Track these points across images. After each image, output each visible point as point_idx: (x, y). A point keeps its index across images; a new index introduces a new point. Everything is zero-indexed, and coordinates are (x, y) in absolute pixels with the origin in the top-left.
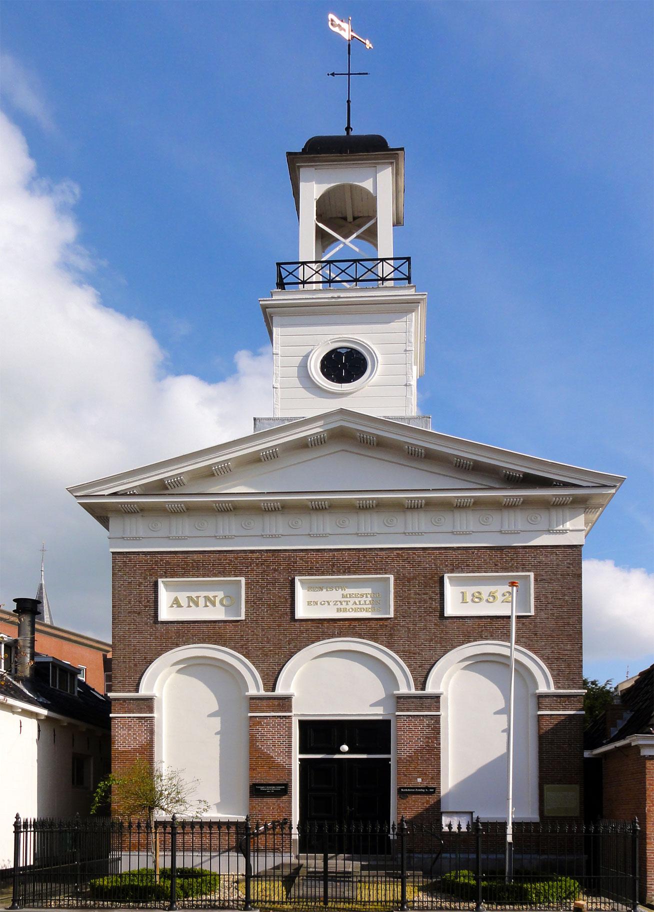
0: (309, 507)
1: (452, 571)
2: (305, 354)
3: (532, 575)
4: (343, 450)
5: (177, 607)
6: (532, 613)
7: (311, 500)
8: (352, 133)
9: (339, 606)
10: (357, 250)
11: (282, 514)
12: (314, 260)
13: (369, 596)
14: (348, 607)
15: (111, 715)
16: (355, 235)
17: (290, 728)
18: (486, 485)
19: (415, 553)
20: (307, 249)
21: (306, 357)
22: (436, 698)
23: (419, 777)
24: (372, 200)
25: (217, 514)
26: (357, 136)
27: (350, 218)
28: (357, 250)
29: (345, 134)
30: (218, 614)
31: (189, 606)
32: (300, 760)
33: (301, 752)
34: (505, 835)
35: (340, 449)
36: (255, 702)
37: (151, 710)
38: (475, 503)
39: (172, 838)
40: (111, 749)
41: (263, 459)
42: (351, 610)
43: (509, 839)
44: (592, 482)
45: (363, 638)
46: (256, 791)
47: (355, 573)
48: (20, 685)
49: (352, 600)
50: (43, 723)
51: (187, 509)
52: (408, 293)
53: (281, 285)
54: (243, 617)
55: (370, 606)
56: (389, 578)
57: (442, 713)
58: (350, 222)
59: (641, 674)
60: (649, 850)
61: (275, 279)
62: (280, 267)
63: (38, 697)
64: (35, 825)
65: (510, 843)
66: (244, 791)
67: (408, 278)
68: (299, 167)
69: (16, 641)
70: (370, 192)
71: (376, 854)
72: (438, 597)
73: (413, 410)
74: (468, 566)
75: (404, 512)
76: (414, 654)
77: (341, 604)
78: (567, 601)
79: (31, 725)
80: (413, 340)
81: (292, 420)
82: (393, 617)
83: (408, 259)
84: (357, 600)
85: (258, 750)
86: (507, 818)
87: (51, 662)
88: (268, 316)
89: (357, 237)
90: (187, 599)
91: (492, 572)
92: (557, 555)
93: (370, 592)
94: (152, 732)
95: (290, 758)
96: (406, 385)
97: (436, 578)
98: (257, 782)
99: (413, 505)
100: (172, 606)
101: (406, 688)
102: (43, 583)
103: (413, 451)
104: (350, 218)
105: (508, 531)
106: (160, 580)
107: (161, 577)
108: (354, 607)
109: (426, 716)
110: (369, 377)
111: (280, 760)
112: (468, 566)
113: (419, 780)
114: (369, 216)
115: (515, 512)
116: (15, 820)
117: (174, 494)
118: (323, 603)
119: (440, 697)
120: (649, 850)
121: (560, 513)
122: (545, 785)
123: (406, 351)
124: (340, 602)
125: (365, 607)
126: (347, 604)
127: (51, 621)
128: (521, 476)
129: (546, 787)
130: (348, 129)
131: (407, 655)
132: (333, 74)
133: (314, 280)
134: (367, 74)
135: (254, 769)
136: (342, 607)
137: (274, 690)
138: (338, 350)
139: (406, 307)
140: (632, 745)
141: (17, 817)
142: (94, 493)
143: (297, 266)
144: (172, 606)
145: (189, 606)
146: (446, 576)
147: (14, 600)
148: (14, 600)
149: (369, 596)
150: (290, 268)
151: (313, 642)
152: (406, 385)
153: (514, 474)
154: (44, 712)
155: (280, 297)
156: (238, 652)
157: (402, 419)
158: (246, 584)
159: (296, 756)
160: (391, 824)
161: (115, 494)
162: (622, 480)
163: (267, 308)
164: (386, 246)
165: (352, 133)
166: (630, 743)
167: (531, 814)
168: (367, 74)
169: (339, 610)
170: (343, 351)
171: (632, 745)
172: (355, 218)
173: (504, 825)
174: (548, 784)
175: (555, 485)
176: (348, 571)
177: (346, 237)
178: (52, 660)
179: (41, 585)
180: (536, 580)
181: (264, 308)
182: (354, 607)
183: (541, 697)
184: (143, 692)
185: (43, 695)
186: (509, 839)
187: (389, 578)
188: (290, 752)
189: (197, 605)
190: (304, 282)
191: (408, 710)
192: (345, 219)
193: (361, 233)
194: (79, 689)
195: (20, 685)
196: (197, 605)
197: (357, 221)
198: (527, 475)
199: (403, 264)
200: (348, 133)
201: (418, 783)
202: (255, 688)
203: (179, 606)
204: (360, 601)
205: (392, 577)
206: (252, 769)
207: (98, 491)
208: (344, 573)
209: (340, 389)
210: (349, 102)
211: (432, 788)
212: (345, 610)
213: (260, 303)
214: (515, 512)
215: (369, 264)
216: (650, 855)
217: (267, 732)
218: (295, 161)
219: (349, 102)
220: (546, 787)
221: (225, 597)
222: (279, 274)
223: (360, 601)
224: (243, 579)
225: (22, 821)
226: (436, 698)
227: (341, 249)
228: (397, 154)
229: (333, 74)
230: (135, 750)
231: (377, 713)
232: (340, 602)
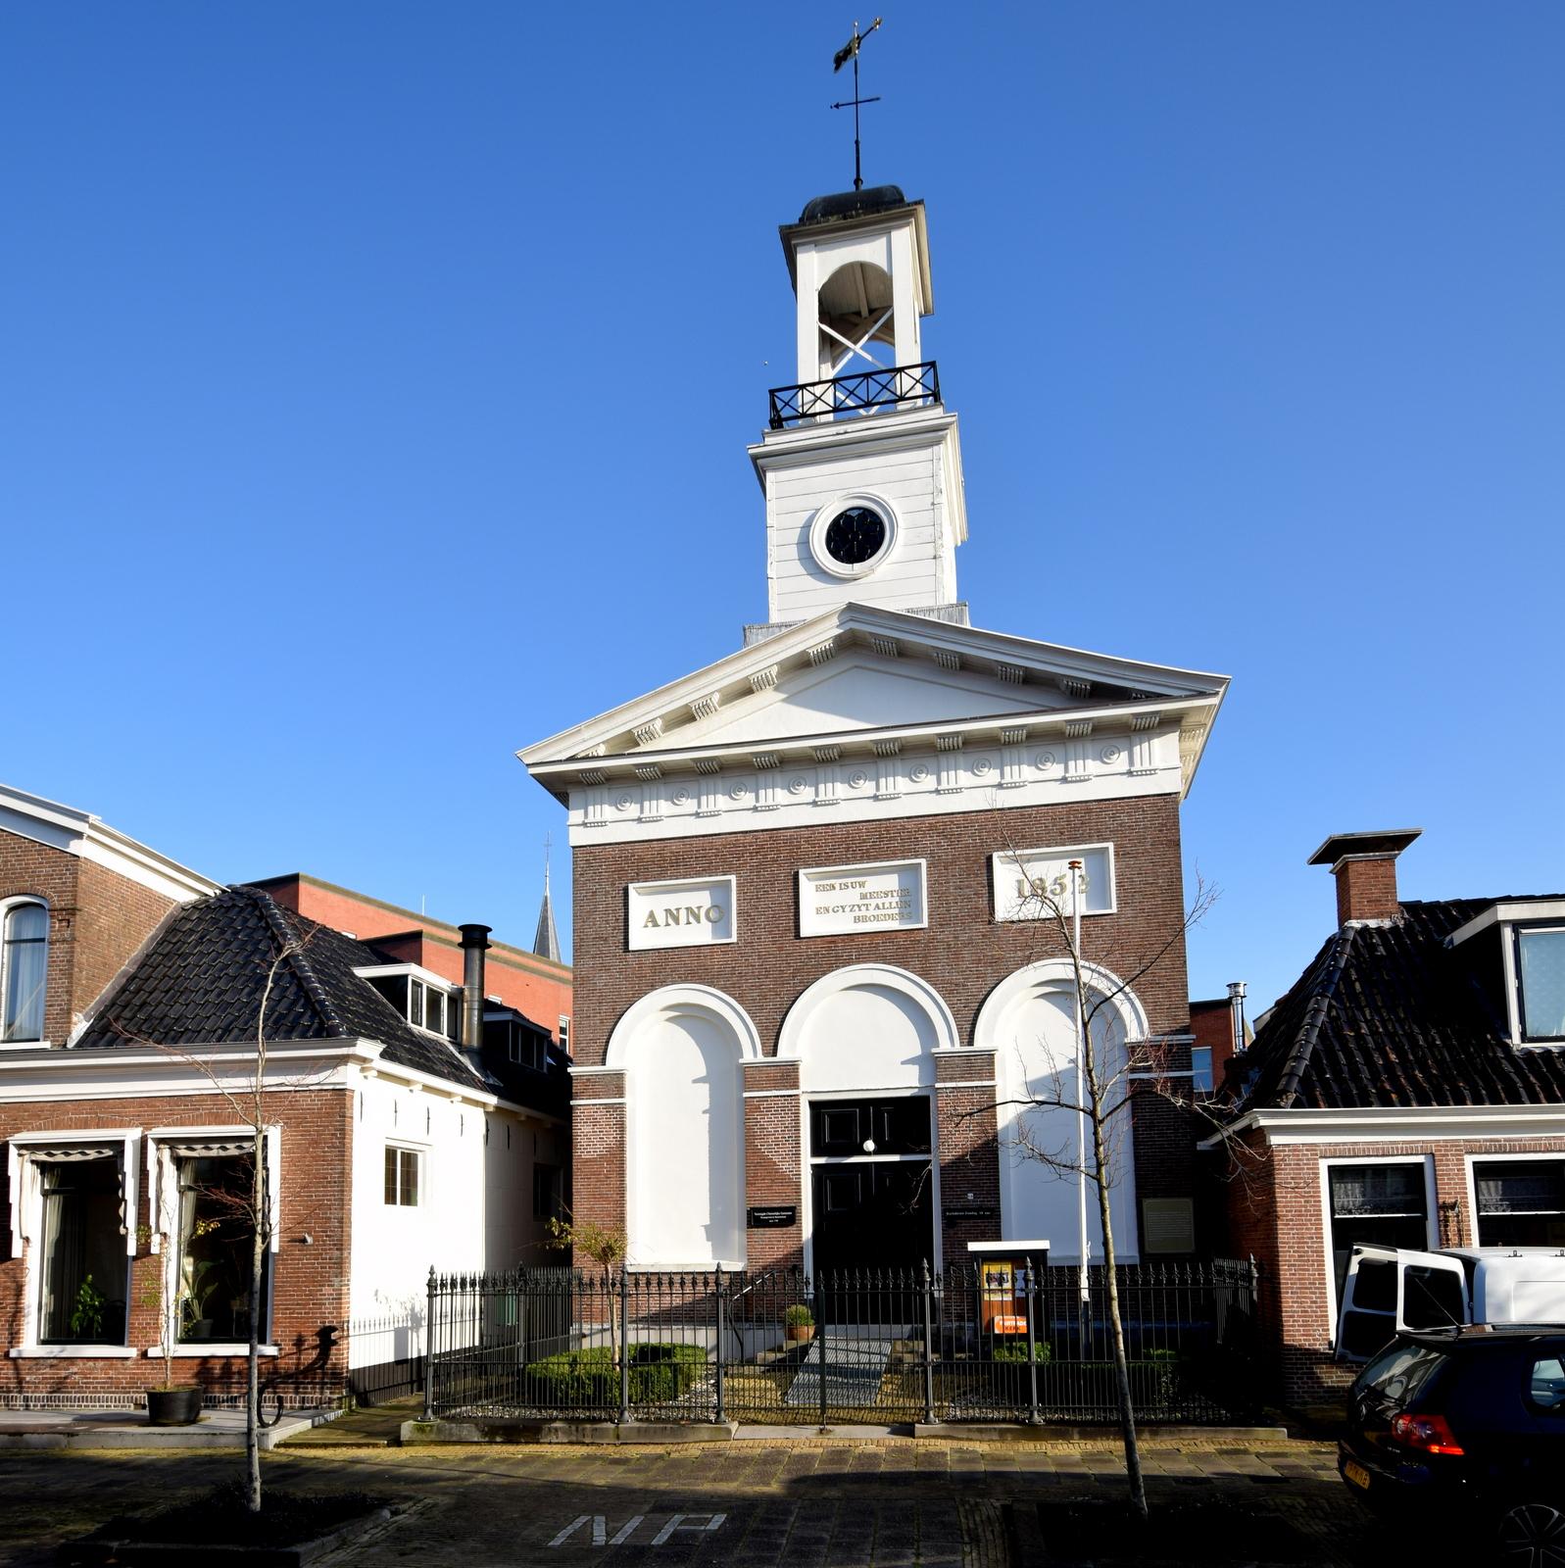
0: (814, 760)
1: (809, 866)
2: (803, 522)
3: (1111, 846)
4: (856, 667)
5: (653, 926)
6: (1114, 910)
7: (816, 748)
8: (863, 187)
9: (857, 913)
10: (869, 358)
11: (841, 766)
12: (920, 362)
13: (895, 894)
14: (868, 914)
15: (572, 1103)
16: (866, 337)
17: (797, 1115)
18: (1043, 706)
19: (952, 822)
20: (810, 365)
21: (807, 527)
22: (988, 1058)
23: (970, 1191)
24: (885, 280)
25: (586, 788)
26: (841, 195)
27: (865, 312)
28: (869, 358)
29: (853, 188)
30: (701, 934)
31: (668, 925)
32: (815, 1167)
33: (815, 1153)
34: (1078, 1290)
35: (846, 668)
36: (750, 1076)
37: (620, 1093)
38: (1030, 736)
39: (623, 1301)
40: (572, 1156)
41: (754, 688)
42: (872, 918)
43: (1085, 1295)
44: (1030, 703)
45: (889, 964)
46: (756, 1219)
47: (876, 859)
48: (465, 1060)
49: (873, 902)
50: (493, 1116)
51: (721, 768)
52: (935, 415)
53: (777, 423)
54: (734, 939)
55: (897, 911)
56: (1107, 848)
57: (627, 1100)
58: (866, 318)
59: (1278, 1003)
60: (1286, 1311)
61: (766, 414)
62: (774, 395)
63: (487, 1076)
64: (484, 1283)
65: (1086, 1303)
66: (738, 1216)
67: (936, 396)
68: (796, 246)
69: (461, 991)
70: (883, 271)
71: (900, 1323)
72: (985, 890)
73: (950, 595)
74: (1023, 837)
75: (1000, 750)
76: (956, 985)
77: (860, 910)
78: (1161, 886)
79: (477, 1121)
80: (943, 487)
81: (791, 626)
82: (927, 926)
83: (772, 392)
84: (880, 902)
85: (756, 1151)
86: (1079, 1258)
87: (511, 1021)
88: (760, 467)
89: (870, 339)
90: (664, 913)
91: (1057, 844)
92: (1143, 811)
93: (896, 887)
94: (621, 1127)
95: (798, 1164)
96: (935, 558)
97: (983, 860)
98: (757, 1205)
99: (955, 745)
100: (646, 926)
101: (948, 1042)
102: (549, 895)
103: (949, 662)
104: (865, 312)
105: (1011, 783)
106: (631, 886)
107: (632, 881)
108: (878, 912)
109: (976, 1087)
110: (884, 554)
111: (785, 1167)
112: (1023, 837)
113: (970, 1196)
114: (883, 308)
115: (947, 758)
116: (429, 1276)
117: (966, 719)
118: (836, 909)
119: (993, 1055)
120: (1286, 1311)
121: (1015, 752)
122: (1144, 1200)
123: (933, 504)
124: (858, 906)
125: (890, 912)
126: (867, 910)
127: (559, 958)
128: (1088, 687)
129: (1146, 1202)
130: (858, 181)
131: (948, 990)
132: (837, 106)
133: (818, 411)
134: (878, 99)
135: (752, 1184)
136: (861, 914)
137: (775, 1054)
138: (848, 513)
139: (931, 436)
140: (1254, 1127)
141: (432, 1272)
142: (552, 755)
143: (795, 391)
144: (646, 926)
145: (668, 925)
146: (995, 855)
147: (1319, 859)
148: (1319, 859)
149: (895, 894)
150: (785, 396)
151: (824, 974)
152: (935, 558)
153: (1070, 684)
154: (492, 1100)
155: (777, 441)
156: (729, 995)
157: (930, 610)
158: (739, 885)
159: (807, 1161)
160: (935, 1273)
161: (572, 759)
162: (1220, 682)
163: (759, 458)
164: (907, 348)
165: (863, 187)
166: (1251, 1125)
167: (1123, 1249)
168: (878, 99)
169: (857, 920)
170: (854, 514)
171: (1254, 1127)
172: (871, 311)
173: (1074, 1271)
174: (1149, 1197)
175: (1135, 698)
176: (867, 857)
177: (855, 343)
178: (511, 1018)
179: (546, 897)
180: (1117, 854)
181: (755, 458)
182: (878, 912)
183: (745, 1069)
184: (613, 1063)
185: (495, 1074)
186: (1085, 1295)
187: (1107, 848)
188: (798, 1154)
189: (677, 921)
190: (902, 398)
191: (952, 1079)
192: (858, 314)
193: (878, 330)
194: (549, 1060)
195: (465, 1060)
196: (677, 921)
197: (875, 314)
198: (1095, 685)
199: (859, 385)
200: (857, 188)
201: (969, 1201)
202: (751, 1053)
203: (656, 925)
204: (883, 904)
205: (923, 862)
206: (749, 1182)
207: (560, 752)
208: (861, 860)
209: (851, 573)
210: (857, 142)
211: (988, 1210)
212: (865, 919)
213: (750, 451)
214: (947, 758)
215: (883, 378)
216: (1289, 1321)
217: (770, 1123)
218: (791, 240)
219: (857, 142)
220: (1146, 1202)
221: (713, 906)
222: (773, 406)
223: (883, 904)
224: (733, 878)
225: (439, 1279)
226: (988, 1058)
227: (850, 360)
228: (915, 209)
229: (837, 106)
230: (601, 1157)
231: (904, 1081)
232: (858, 906)
